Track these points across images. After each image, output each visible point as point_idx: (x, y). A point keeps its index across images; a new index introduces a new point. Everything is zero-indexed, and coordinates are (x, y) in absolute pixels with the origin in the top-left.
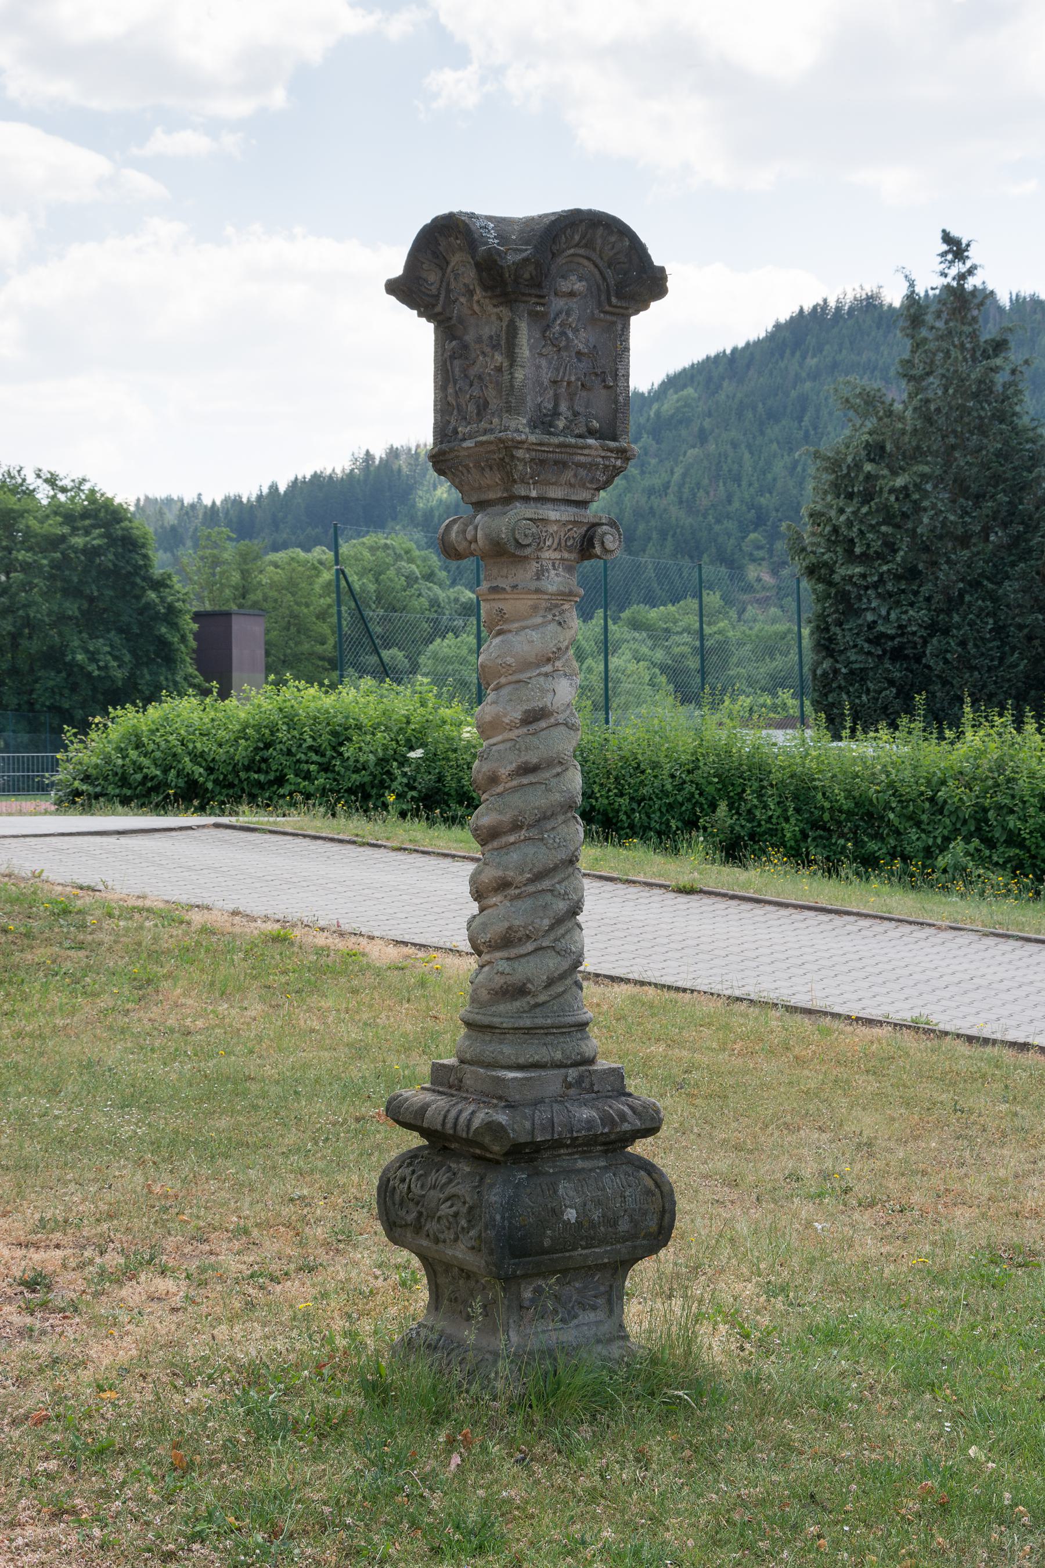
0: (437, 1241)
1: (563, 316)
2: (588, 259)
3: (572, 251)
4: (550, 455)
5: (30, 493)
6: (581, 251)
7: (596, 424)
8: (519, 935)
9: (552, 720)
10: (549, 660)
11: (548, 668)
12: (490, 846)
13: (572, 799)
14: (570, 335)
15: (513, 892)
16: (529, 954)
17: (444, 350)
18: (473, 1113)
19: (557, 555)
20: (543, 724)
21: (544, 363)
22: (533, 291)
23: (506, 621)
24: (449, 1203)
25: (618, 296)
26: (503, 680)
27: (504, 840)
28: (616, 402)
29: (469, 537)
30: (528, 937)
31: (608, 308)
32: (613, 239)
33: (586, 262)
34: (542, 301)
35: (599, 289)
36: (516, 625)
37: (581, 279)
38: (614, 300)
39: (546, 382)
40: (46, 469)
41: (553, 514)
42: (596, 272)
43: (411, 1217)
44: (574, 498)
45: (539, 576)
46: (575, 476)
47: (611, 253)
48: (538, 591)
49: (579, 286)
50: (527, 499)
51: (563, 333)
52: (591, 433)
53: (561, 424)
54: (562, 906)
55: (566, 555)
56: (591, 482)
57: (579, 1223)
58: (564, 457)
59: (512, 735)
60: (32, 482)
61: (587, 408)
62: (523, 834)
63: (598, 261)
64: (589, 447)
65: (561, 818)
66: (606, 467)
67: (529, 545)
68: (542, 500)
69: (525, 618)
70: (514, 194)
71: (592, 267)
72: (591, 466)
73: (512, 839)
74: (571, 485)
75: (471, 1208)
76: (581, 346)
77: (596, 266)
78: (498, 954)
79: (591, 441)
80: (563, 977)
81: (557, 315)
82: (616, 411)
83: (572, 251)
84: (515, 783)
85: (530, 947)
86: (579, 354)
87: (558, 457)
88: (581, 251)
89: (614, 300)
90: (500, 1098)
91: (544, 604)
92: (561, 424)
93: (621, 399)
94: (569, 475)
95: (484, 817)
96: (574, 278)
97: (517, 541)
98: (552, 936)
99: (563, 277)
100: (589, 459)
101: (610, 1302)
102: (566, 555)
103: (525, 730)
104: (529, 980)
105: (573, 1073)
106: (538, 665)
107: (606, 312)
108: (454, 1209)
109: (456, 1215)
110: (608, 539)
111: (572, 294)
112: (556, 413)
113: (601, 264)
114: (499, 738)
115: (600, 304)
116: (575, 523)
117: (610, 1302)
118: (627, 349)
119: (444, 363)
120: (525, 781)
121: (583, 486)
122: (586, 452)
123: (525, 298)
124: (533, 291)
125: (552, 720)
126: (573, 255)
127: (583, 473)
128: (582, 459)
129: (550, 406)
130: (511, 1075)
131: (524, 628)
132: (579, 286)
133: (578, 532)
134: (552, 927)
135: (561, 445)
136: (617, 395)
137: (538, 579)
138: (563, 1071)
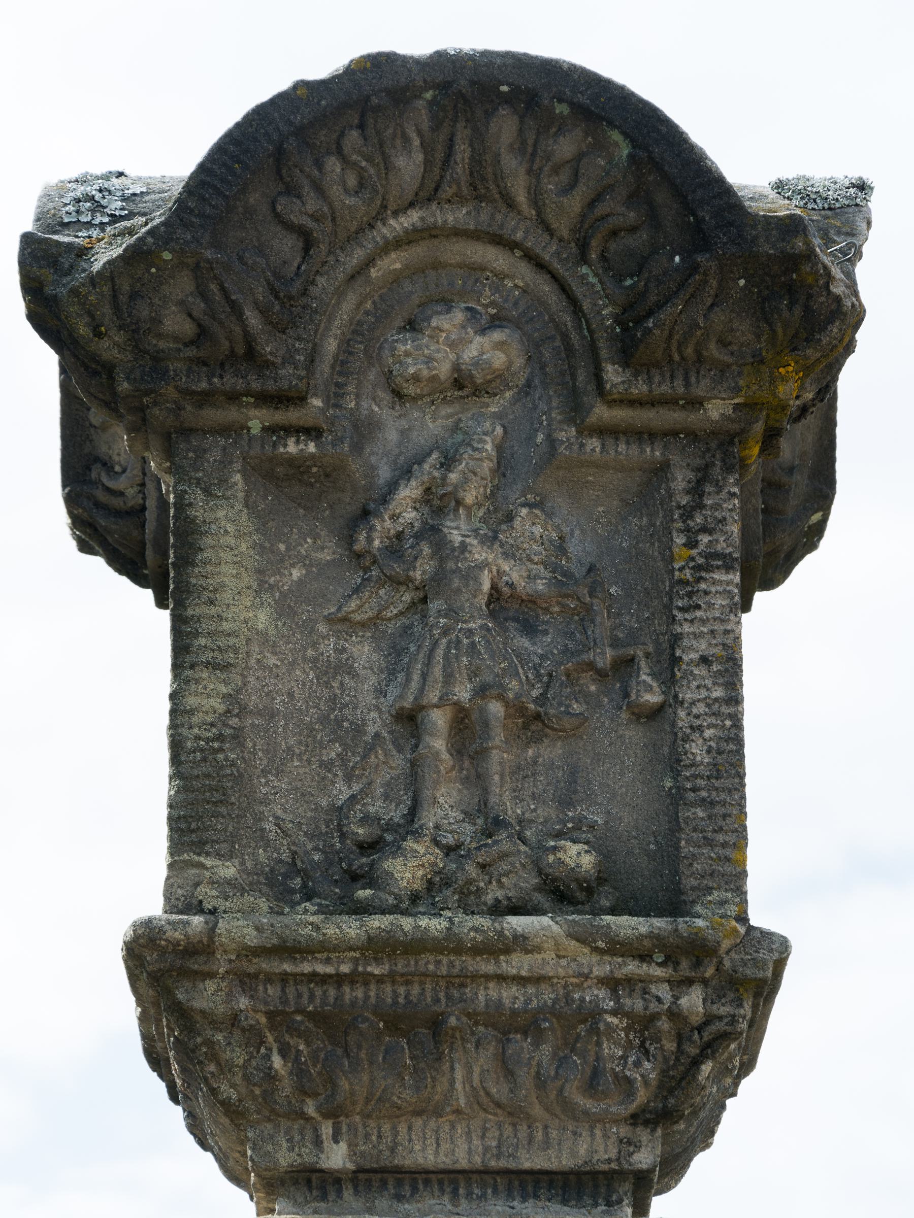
2: (498, 240)
6: (455, 216)
22: (231, 382)
25: (627, 356)
28: (675, 763)
31: (601, 413)
32: (565, 147)
34: (292, 416)
35: (569, 349)
38: (613, 374)
39: (375, 724)
42: (546, 287)
44: (529, 1161)
47: (575, 203)
49: (489, 351)
51: (431, 532)
52: (562, 893)
61: (565, 802)
63: (537, 242)
64: (520, 943)
71: (525, 274)
77: (540, 265)
88: (455, 216)
89: (613, 374)
93: (697, 750)
94: (467, 1072)
96: (449, 322)
99: (412, 326)
107: (604, 431)
111: (464, 384)
113: (548, 252)
115: (575, 412)
123: (214, 415)
124: (231, 382)
128: (511, 996)
132: (489, 351)
136: (678, 740)
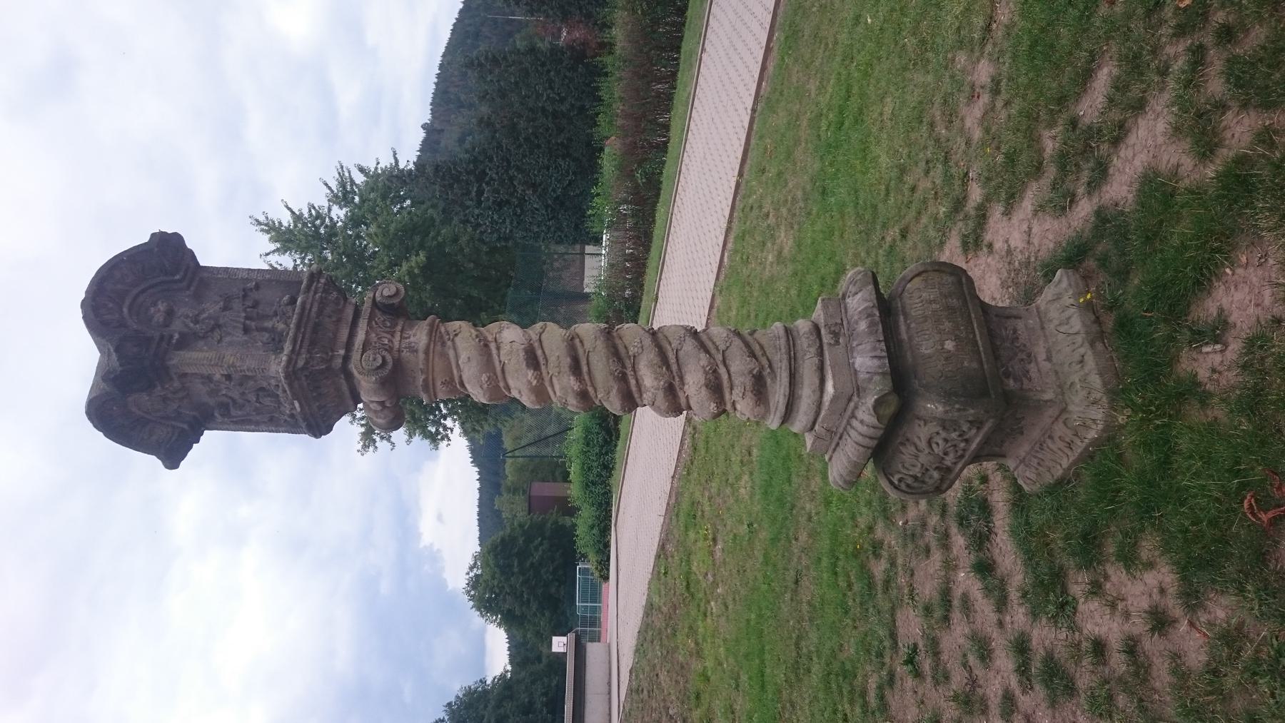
0: (962, 456)
1: (188, 321)
3: (125, 310)
4: (307, 336)
5: (476, 576)
6: (127, 302)
7: (286, 298)
8: (712, 378)
9: (536, 345)
10: (486, 346)
11: (493, 346)
12: (638, 400)
13: (602, 331)
14: (205, 315)
15: (677, 382)
16: (728, 372)
17: (222, 423)
18: (862, 422)
19: (398, 335)
20: (539, 352)
21: (228, 339)
23: (452, 379)
24: (934, 446)
26: (502, 384)
27: (634, 389)
29: (379, 408)
30: (715, 371)
31: (185, 284)
33: (141, 299)
36: (455, 372)
37: (155, 304)
38: (177, 277)
39: (245, 338)
40: (467, 570)
41: (360, 336)
42: (151, 291)
43: (936, 475)
45: (414, 351)
46: (330, 317)
48: (427, 352)
50: (346, 358)
53: (281, 326)
54: (689, 345)
55: (399, 328)
56: (337, 304)
57: (957, 338)
58: (311, 324)
59: (547, 379)
60: (472, 574)
62: (629, 372)
64: (304, 303)
65: (618, 342)
66: (325, 291)
67: (384, 358)
68: (349, 345)
69: (450, 363)
70: (79, 359)
72: (323, 303)
73: (633, 382)
74: (339, 320)
75: (944, 428)
76: (217, 307)
78: (727, 396)
79: (299, 300)
80: (747, 345)
81: (186, 326)
82: (277, 281)
83: (125, 310)
84: (586, 377)
85: (722, 370)
86: (225, 308)
87: (309, 330)
90: (850, 400)
91: (438, 348)
92: (281, 326)
95: (613, 405)
97: (378, 368)
98: (713, 351)
100: (316, 305)
101: (1008, 317)
102: (399, 328)
103: (543, 367)
104: (751, 372)
105: (826, 338)
106: (490, 355)
108: (940, 442)
109: (946, 440)
110: (386, 293)
112: (272, 330)
114: (549, 389)
116: (370, 319)
117: (1008, 317)
118: (226, 270)
119: (236, 423)
120: (585, 369)
121: (341, 311)
122: (308, 306)
125: (536, 345)
126: (130, 310)
127: (328, 310)
128: (315, 309)
129: (267, 335)
130: (830, 388)
131: (458, 365)
132: (162, 306)
133: (380, 317)
134: (707, 351)
135: (298, 326)
137: (416, 351)
138: (826, 348)
